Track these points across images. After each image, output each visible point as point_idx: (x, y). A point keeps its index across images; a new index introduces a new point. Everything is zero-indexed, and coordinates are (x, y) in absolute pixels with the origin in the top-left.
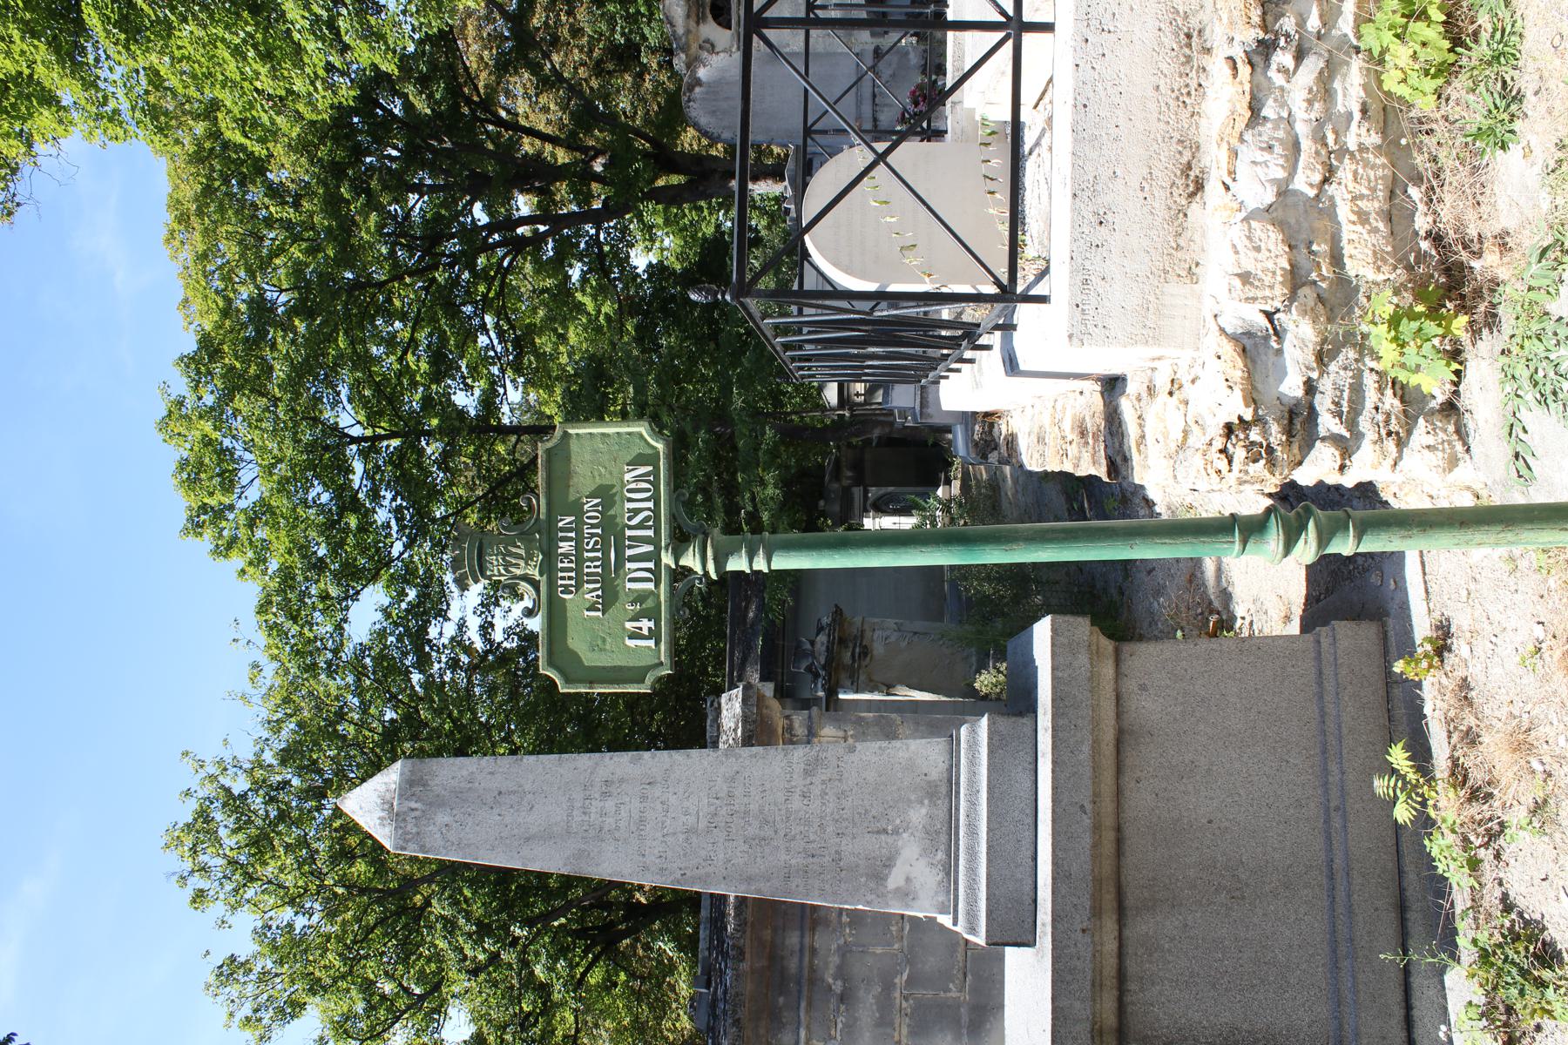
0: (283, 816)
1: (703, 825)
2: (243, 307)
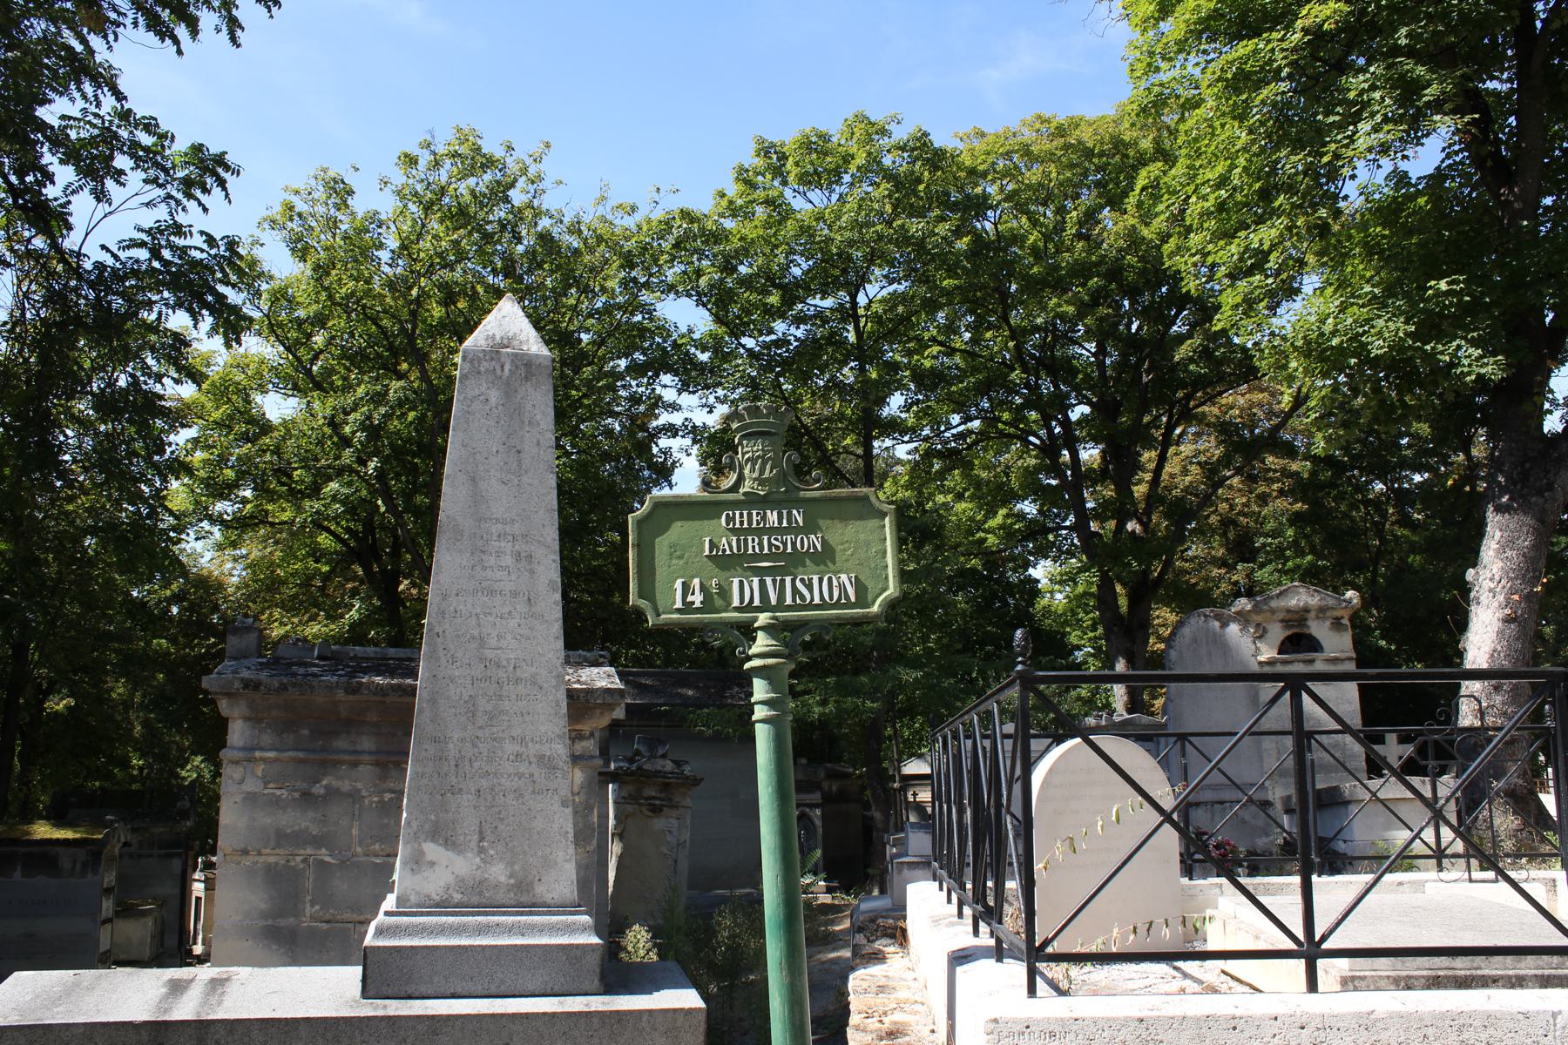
0: (487, 237)
1: (489, 654)
2: (979, 190)
